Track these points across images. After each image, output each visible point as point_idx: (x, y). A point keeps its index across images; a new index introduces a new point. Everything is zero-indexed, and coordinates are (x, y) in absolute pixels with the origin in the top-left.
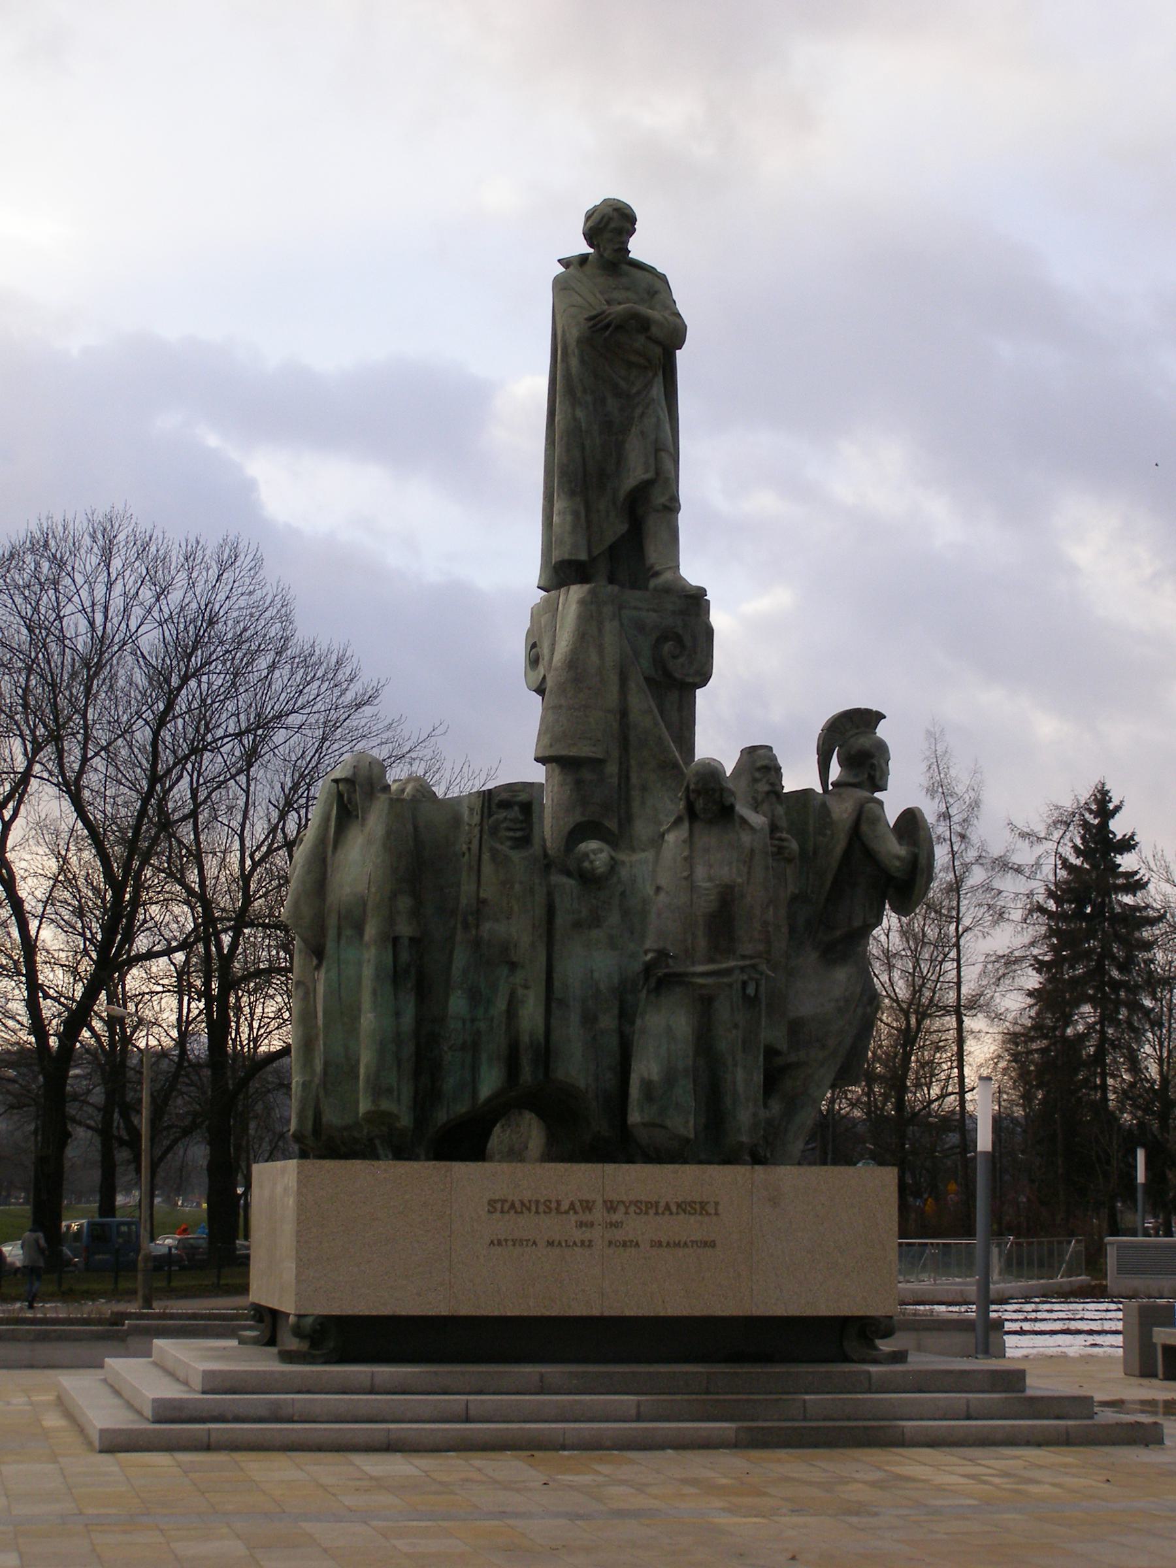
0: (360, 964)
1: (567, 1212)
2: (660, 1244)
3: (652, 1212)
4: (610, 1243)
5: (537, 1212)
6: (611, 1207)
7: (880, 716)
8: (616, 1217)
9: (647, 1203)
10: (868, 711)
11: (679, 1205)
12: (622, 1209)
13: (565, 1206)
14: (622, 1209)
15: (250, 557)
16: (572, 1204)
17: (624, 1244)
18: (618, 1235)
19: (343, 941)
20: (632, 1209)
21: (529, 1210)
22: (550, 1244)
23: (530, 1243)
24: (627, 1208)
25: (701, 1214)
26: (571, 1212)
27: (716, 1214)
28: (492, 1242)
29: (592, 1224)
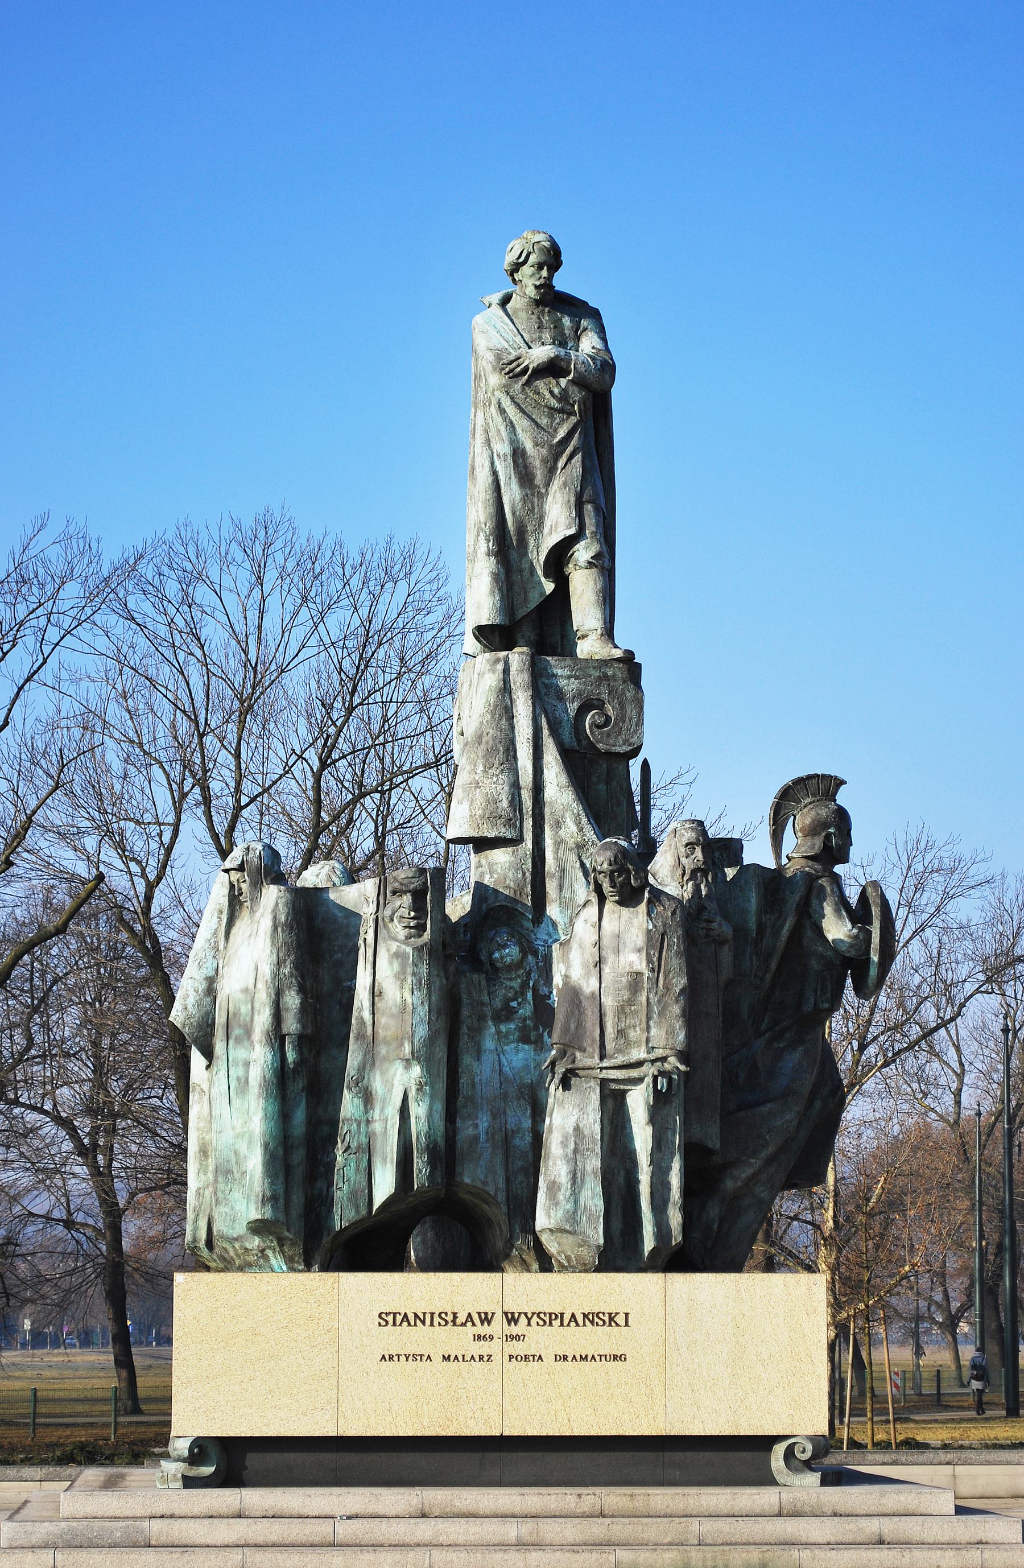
0: (247, 1064)
1: (464, 1325)
2: (565, 1358)
3: (556, 1323)
4: (511, 1357)
5: (432, 1324)
6: (511, 1319)
7: (843, 782)
8: (514, 1330)
9: (550, 1314)
10: (836, 778)
11: (585, 1316)
12: (523, 1320)
13: (462, 1318)
14: (523, 1320)
15: (429, 567)
16: (573, 1316)
17: (526, 1358)
18: (518, 1348)
19: (231, 1042)
20: (535, 1319)
21: (423, 1322)
22: (446, 1358)
23: (536, 1358)
24: (529, 1320)
25: (610, 1325)
26: (469, 1324)
27: (627, 1325)
28: (383, 1357)
29: (491, 1338)
